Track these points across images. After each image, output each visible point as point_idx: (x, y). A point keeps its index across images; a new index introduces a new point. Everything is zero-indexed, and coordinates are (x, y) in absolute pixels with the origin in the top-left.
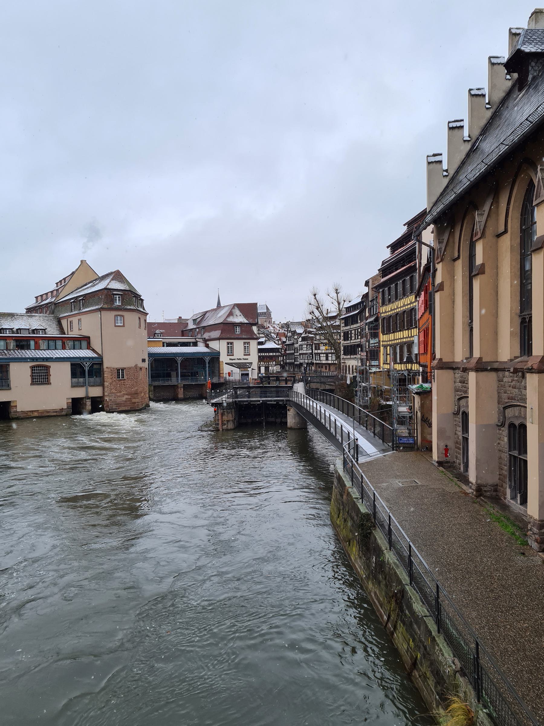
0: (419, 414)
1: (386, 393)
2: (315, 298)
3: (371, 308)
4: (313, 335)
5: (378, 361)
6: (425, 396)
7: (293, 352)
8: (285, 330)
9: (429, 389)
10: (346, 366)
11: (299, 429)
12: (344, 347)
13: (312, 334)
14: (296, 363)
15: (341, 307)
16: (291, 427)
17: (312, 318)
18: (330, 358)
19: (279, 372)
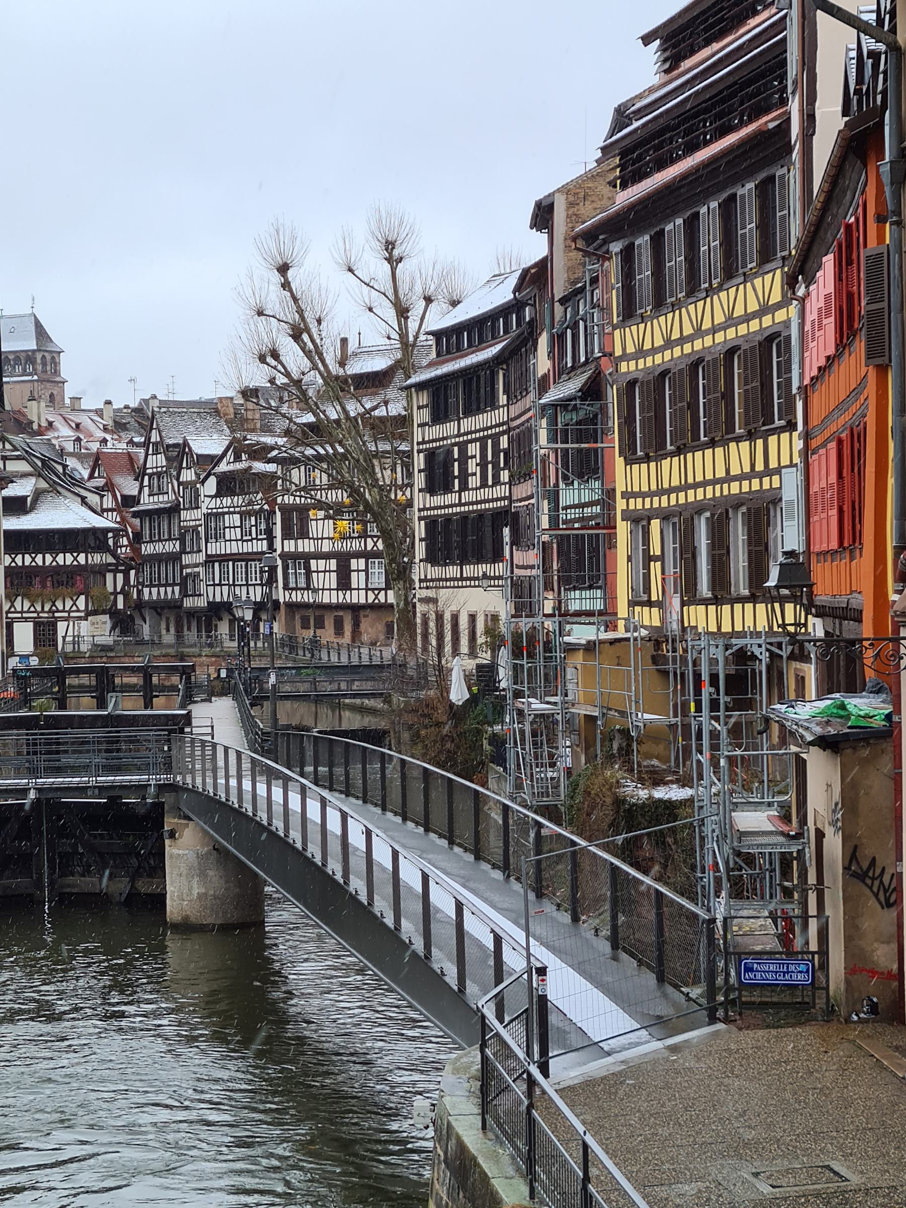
0: (834, 844)
1: (644, 748)
2: (286, 285)
3: (562, 337)
4: (271, 467)
5: (599, 593)
6: (866, 752)
7: (172, 547)
8: (131, 442)
9: (878, 723)
10: (440, 617)
11: (225, 928)
12: (431, 524)
13: (269, 461)
14: (188, 603)
15: (413, 325)
16: (187, 918)
17: (272, 381)
18: (357, 579)
19: (105, 648)
